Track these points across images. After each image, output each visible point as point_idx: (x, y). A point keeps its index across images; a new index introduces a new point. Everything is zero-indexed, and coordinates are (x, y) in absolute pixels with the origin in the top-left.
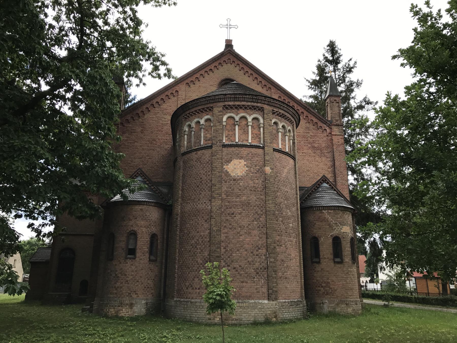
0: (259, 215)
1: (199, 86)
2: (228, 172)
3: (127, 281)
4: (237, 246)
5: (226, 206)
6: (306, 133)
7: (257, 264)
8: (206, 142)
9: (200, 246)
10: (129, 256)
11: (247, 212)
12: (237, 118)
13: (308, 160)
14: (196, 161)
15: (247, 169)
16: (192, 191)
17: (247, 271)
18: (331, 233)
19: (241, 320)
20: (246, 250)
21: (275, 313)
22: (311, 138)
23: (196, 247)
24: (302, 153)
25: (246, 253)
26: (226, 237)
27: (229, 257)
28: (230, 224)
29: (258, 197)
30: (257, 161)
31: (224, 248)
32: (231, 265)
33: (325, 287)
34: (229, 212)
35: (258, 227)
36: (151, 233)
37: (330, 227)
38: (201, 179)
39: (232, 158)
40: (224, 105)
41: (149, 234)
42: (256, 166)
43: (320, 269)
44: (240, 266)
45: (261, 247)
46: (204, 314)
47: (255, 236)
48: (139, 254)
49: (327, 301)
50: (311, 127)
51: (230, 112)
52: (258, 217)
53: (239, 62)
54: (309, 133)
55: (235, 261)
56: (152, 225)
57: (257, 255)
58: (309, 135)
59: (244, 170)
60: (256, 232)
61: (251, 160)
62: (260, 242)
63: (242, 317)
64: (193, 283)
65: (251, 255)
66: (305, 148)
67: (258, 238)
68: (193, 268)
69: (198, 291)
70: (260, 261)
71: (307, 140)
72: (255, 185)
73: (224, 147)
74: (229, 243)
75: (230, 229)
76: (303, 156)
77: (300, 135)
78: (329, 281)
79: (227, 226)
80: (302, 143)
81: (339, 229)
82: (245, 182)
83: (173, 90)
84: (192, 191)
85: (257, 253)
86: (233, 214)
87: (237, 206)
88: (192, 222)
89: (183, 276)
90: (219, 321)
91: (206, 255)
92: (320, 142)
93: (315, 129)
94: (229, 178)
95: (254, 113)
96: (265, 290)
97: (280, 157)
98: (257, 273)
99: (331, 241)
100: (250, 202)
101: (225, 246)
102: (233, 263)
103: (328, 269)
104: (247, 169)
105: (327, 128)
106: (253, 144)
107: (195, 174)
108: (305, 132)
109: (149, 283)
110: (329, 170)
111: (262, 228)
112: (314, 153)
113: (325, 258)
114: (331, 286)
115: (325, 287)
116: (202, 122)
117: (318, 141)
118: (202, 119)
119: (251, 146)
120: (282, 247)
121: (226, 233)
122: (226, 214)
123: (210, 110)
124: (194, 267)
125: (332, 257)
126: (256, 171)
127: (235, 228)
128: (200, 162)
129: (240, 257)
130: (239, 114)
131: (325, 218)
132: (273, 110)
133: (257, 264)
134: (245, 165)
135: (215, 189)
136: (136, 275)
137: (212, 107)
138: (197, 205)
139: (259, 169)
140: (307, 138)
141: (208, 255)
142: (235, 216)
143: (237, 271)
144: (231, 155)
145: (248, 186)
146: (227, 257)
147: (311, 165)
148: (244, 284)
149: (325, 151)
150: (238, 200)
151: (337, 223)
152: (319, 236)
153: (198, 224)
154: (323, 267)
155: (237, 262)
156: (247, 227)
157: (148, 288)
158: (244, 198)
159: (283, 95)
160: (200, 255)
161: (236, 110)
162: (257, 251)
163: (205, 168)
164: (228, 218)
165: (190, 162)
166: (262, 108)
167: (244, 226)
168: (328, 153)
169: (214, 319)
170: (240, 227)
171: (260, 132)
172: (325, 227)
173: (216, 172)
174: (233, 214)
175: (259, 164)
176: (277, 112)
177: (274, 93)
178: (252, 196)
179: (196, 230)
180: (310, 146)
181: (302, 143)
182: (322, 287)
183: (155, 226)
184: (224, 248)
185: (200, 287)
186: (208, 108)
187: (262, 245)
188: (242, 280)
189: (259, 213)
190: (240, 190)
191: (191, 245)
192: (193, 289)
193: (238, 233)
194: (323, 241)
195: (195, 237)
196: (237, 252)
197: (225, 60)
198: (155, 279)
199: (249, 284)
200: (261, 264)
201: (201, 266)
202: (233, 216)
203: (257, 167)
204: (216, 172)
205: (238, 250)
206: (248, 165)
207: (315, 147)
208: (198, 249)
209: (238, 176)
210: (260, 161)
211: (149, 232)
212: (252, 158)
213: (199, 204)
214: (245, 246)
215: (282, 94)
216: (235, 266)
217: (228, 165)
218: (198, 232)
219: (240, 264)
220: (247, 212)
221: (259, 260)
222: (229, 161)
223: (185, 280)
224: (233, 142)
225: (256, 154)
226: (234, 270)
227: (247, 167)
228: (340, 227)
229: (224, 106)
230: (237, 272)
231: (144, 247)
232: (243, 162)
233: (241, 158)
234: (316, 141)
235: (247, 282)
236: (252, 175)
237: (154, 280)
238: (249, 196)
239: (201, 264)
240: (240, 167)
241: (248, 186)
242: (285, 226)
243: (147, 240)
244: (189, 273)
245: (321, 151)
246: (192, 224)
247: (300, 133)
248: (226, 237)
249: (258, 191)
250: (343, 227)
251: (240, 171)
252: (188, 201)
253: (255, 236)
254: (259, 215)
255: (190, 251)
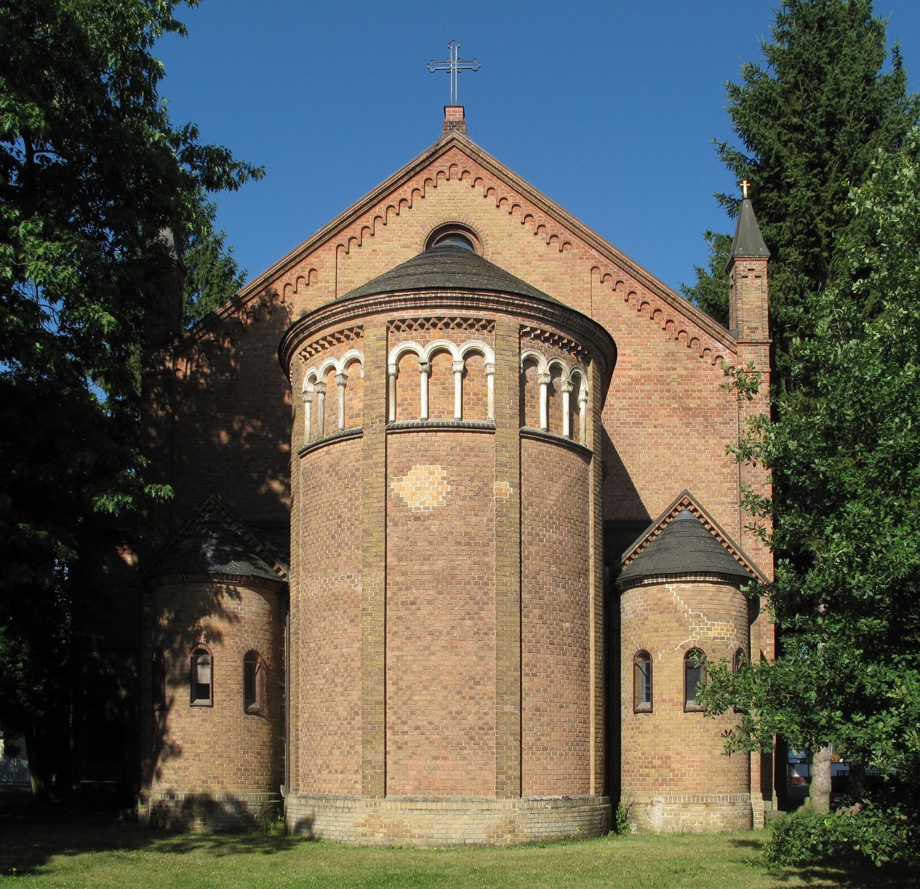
0: (477, 603)
1: (374, 251)
2: (401, 500)
3: (197, 755)
4: (424, 678)
5: (398, 584)
6: (668, 369)
7: (471, 719)
8: (351, 422)
9: (341, 680)
10: (198, 701)
11: (448, 597)
12: (424, 355)
13: (669, 446)
14: (328, 472)
15: (449, 488)
16: (322, 549)
17: (446, 733)
18: (682, 639)
19: (432, 837)
20: (445, 688)
21: (511, 822)
22: (679, 384)
23: (333, 681)
24: (655, 427)
25: (444, 693)
26: (398, 657)
27: (404, 703)
28: (408, 628)
29: (477, 559)
30: (476, 466)
31: (394, 684)
32: (409, 722)
33: (660, 767)
34: (404, 599)
35: (476, 633)
36: (243, 648)
37: (680, 625)
38: (339, 517)
39: (410, 460)
40: (390, 319)
41: (239, 652)
42: (472, 480)
43: (651, 727)
44: (430, 723)
45: (482, 679)
46: (351, 824)
47: (467, 653)
48: (218, 695)
49: (661, 799)
50: (681, 348)
51: (406, 339)
52: (476, 608)
53: (483, 173)
54: (674, 369)
55: (418, 712)
56: (246, 631)
57: (471, 698)
58: (674, 375)
59: (441, 493)
60: (470, 645)
61: (459, 465)
62: (479, 668)
63: (432, 831)
64: (330, 761)
65: (457, 697)
66: (661, 412)
67: (474, 658)
68: (330, 728)
69: (340, 776)
70: (478, 712)
71: (669, 391)
72: (469, 529)
73: (391, 434)
74: (404, 672)
75: (407, 639)
76: (657, 434)
77: (649, 376)
78: (671, 753)
79: (400, 633)
80: (655, 397)
81: (703, 629)
82: (444, 522)
83: (303, 269)
84: (322, 549)
85: (473, 692)
86: (413, 603)
87: (423, 583)
88: (323, 625)
89: (310, 744)
90: (383, 840)
91: (355, 699)
92: (705, 394)
93: (693, 358)
94: (403, 514)
95: (468, 338)
96: (491, 777)
97: (541, 453)
98: (472, 738)
99: (680, 660)
100: (456, 572)
101: (395, 678)
102: (414, 717)
103: (668, 727)
104: (449, 488)
105: (725, 353)
106: (465, 421)
107: (327, 505)
108: (665, 365)
109: (247, 761)
110: (725, 471)
111: (485, 634)
112: (688, 424)
113: (664, 701)
114: (674, 766)
115: (660, 767)
116: (340, 366)
117: (700, 391)
118: (338, 359)
119: (459, 428)
120: (535, 679)
121: (398, 649)
122: (396, 604)
123: (358, 335)
124: (331, 725)
125: (681, 697)
126: (471, 494)
127: (419, 637)
128: (337, 474)
129: (431, 702)
130: (428, 341)
131: (670, 603)
132: (522, 327)
133: (469, 718)
134: (444, 478)
135: (371, 542)
136: (215, 743)
137: (361, 327)
138: (333, 584)
139: (481, 489)
140: (669, 384)
141: (359, 699)
142: (419, 609)
143: (423, 734)
144: (407, 454)
145: (451, 533)
146: (400, 703)
147: (677, 460)
148: (439, 762)
149: (716, 419)
150: (425, 568)
151: (698, 616)
152: (653, 648)
153: (336, 627)
154: (657, 722)
155: (423, 713)
156: (448, 633)
157: (246, 770)
158: (440, 562)
159: (606, 261)
160: (342, 698)
161: (422, 332)
162: (472, 688)
163: (348, 490)
164: (403, 612)
165: (316, 475)
166: (489, 322)
167: (441, 632)
168: (725, 423)
169: (373, 835)
170: (431, 634)
171: (486, 386)
172: (669, 625)
173: (371, 500)
174: (413, 603)
175: (482, 474)
176: (533, 329)
177: (581, 258)
178: (461, 558)
179: (332, 642)
180: (676, 406)
181: (655, 397)
182: (653, 767)
183: (252, 632)
184: (394, 684)
185: (344, 768)
186: (351, 330)
187: (485, 674)
188: (434, 754)
189: (478, 598)
190: (431, 543)
191: (324, 677)
192: (330, 772)
193: (426, 648)
194: (663, 661)
195: (331, 657)
196: (424, 692)
197: (441, 169)
198: (263, 753)
199: (452, 763)
200: (480, 718)
201: (345, 722)
202: (414, 607)
203: (474, 484)
204: (371, 500)
205: (425, 688)
206: (452, 478)
207: (690, 409)
208: (336, 686)
209: (425, 508)
210: (484, 466)
211: (237, 647)
212: (463, 460)
213: (336, 579)
214: (442, 677)
215: (602, 258)
216: (419, 724)
217: (401, 480)
218: (336, 648)
219: (431, 718)
220: (448, 597)
221: (474, 709)
222: (403, 471)
223: (315, 753)
224: (416, 418)
225: (472, 449)
226: (416, 733)
227: (449, 483)
228: (707, 624)
229: (391, 322)
230: (424, 737)
231: (229, 682)
232: (439, 471)
233: (435, 460)
234: (693, 391)
235: (445, 758)
236: (461, 503)
237: (259, 753)
238: (454, 558)
239: (346, 719)
240: (432, 483)
241: (451, 533)
242: (547, 628)
243: (235, 664)
244: (321, 738)
245: (706, 419)
246: (324, 629)
247: (649, 369)
248: (398, 657)
249: (476, 544)
250: (714, 625)
251: (431, 494)
252: (314, 574)
253: (467, 653)
254: (477, 603)
255: (322, 690)
